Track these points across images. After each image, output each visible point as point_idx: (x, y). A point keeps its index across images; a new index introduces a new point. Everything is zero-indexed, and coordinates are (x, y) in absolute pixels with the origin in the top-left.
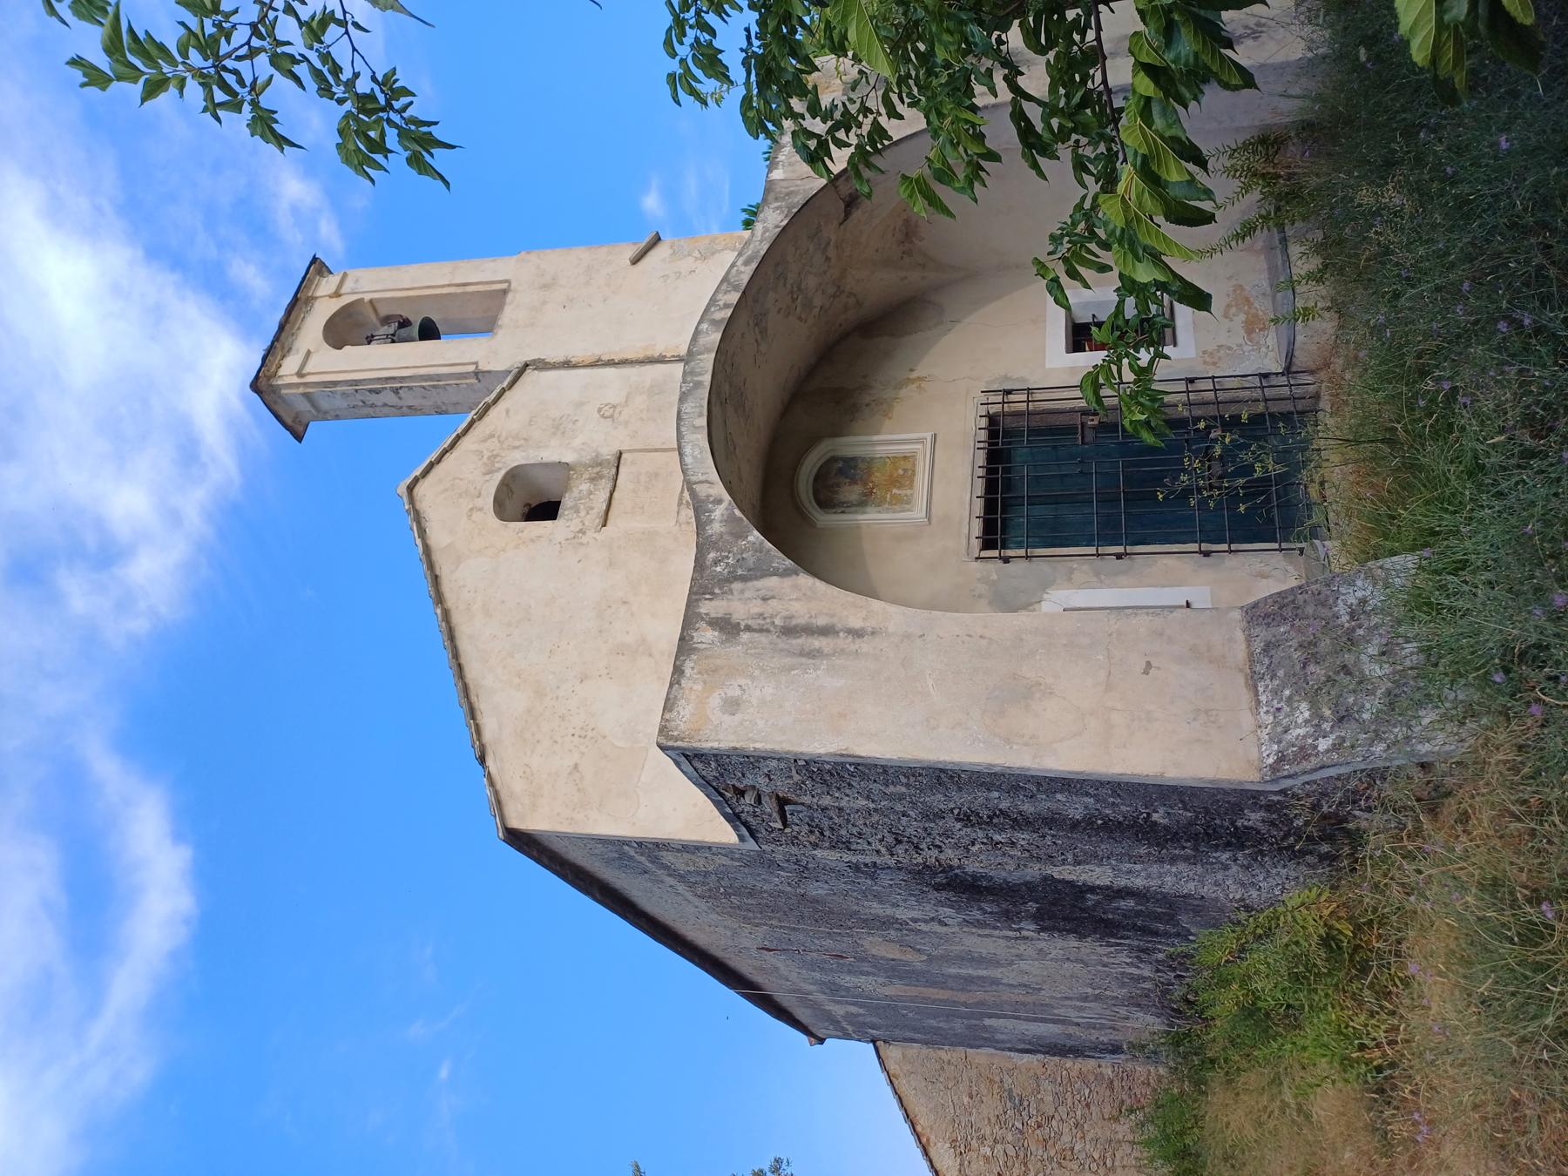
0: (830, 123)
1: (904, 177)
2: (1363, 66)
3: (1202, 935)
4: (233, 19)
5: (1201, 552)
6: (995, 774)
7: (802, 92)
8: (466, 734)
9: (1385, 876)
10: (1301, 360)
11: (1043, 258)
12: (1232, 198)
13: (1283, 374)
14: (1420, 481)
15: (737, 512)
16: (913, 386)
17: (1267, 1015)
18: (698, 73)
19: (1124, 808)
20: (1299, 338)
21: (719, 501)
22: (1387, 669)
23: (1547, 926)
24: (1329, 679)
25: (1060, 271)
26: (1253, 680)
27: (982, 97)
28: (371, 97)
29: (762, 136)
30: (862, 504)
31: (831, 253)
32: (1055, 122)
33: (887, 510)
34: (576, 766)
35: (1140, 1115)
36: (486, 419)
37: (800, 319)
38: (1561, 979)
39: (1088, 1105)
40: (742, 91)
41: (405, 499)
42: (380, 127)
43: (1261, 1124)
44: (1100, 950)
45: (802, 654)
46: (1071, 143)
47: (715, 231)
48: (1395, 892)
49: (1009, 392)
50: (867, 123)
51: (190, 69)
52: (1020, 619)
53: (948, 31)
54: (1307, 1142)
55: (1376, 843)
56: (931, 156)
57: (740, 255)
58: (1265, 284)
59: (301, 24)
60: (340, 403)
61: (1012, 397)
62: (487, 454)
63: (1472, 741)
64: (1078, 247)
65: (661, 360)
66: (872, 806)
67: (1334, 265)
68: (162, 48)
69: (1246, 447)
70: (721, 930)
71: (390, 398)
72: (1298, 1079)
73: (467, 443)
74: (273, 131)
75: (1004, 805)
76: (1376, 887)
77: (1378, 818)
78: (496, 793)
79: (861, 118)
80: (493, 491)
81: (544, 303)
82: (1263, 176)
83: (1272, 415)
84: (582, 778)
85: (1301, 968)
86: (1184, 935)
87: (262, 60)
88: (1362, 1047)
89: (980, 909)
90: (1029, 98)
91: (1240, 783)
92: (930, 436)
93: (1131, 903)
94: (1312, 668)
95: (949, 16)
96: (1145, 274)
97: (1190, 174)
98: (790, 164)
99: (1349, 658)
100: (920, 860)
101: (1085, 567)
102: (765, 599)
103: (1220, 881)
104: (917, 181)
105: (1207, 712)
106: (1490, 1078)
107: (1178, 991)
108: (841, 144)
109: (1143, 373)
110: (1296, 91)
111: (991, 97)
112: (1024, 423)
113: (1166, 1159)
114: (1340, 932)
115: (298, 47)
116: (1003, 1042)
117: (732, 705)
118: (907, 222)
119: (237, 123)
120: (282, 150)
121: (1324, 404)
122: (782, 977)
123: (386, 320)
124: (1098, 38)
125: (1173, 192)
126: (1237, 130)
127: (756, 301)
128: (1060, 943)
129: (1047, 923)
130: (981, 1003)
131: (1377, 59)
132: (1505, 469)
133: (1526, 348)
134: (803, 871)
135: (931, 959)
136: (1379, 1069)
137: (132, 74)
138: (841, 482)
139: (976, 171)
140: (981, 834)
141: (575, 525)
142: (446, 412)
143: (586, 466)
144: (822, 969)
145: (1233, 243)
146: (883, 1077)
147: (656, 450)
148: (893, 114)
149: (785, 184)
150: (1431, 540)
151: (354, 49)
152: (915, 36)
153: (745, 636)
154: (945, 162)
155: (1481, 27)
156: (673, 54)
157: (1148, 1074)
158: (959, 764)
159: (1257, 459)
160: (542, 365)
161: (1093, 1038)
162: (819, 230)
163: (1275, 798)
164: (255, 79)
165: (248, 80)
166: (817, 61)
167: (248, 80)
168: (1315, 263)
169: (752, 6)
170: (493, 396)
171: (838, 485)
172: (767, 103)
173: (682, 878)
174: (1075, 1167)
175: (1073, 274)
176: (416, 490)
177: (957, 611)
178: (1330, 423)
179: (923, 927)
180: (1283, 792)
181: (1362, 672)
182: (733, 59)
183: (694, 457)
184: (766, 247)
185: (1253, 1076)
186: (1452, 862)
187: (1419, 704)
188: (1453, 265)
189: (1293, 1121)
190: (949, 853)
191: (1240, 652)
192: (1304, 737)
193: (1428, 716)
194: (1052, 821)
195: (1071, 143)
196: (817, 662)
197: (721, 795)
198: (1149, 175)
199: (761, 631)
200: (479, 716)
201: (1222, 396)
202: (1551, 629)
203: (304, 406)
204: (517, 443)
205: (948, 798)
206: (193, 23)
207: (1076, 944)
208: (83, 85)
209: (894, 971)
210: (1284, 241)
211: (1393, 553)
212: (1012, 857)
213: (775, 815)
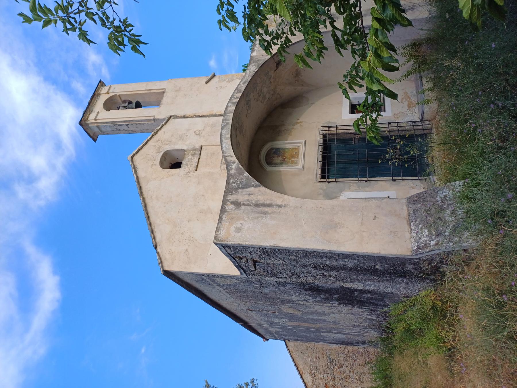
0: (272, 37)
1: (296, 55)
3: (392, 305)
5: (393, 180)
7: (263, 26)
8: (150, 239)
9: (452, 286)
10: (426, 117)
11: (342, 82)
12: (405, 63)
13: (420, 121)
15: (240, 166)
16: (298, 125)
17: (413, 331)
18: (228, 20)
19: (367, 264)
20: (426, 110)
21: (234, 162)
22: (453, 218)
23: (505, 303)
24: (434, 222)
26: (409, 222)
28: (119, 27)
29: (249, 41)
31: (272, 80)
32: (346, 37)
34: (187, 250)
36: (157, 135)
37: (261, 102)
38: (509, 320)
39: (355, 361)
41: (130, 161)
42: (122, 37)
43: (411, 367)
44: (359, 310)
45: (261, 213)
46: (351, 44)
47: (234, 73)
48: (455, 291)
49: (330, 127)
50: (284, 37)
51: (59, 17)
54: (426, 373)
56: (305, 48)
57: (242, 81)
58: (415, 92)
60: (109, 129)
61: (331, 129)
62: (157, 146)
64: (353, 79)
65: (215, 115)
66: (284, 263)
68: (49, 10)
70: (234, 304)
71: (126, 128)
72: (423, 353)
73: (150, 143)
75: (328, 263)
77: (450, 267)
78: (160, 259)
79: (282, 35)
80: (159, 158)
81: (177, 96)
82: (414, 56)
83: (416, 135)
86: (386, 306)
87: (83, 14)
88: (444, 342)
89: (320, 297)
91: (405, 256)
92: (304, 142)
93: (368, 295)
94: (429, 218)
96: (375, 87)
98: (259, 51)
99: (441, 215)
100: (300, 281)
101: (355, 185)
102: (249, 195)
103: (398, 288)
104: (300, 57)
105: (394, 232)
107: (384, 324)
108: (275, 44)
109: (374, 121)
110: (427, 28)
111: (325, 29)
113: (380, 379)
114: (437, 304)
115: (95, 10)
118: (297, 70)
119: (74, 35)
120: (89, 44)
121: (434, 131)
122: (255, 319)
123: (124, 102)
124: (360, 10)
125: (384, 60)
126: (407, 40)
127: (247, 96)
130: (320, 328)
131: (452, 17)
132: (492, 153)
133: (500, 113)
134: (262, 284)
135: (303, 313)
136: (450, 349)
137: (39, 19)
138: (275, 156)
139: (320, 53)
140: (320, 272)
141: (187, 170)
143: (190, 151)
145: (404, 78)
146: (287, 352)
147: (214, 145)
148: (293, 34)
149: (257, 57)
150: (468, 176)
151: (114, 11)
152: (300, 8)
153: (243, 207)
155: (486, 6)
156: (220, 14)
158: (313, 249)
159: (411, 149)
160: (176, 117)
163: (417, 261)
164: (80, 21)
165: (78, 21)
166: (268, 17)
167: (78, 21)
168: (431, 85)
170: (159, 127)
171: (274, 157)
172: (251, 30)
173: (222, 287)
174: (350, 381)
175: (351, 88)
176: (134, 158)
179: (301, 303)
180: (419, 259)
181: (445, 219)
182: (239, 15)
183: (226, 148)
184: (250, 78)
185: (409, 352)
186: (474, 281)
187: (464, 230)
188: (476, 86)
189: (422, 366)
190: (310, 278)
191: (405, 213)
192: (426, 241)
193: (467, 234)
194: (343, 268)
195: (351, 44)
196: (266, 216)
197: (235, 259)
198: (377, 54)
199: (248, 205)
200: (154, 233)
201: (400, 128)
202: (507, 205)
203: (97, 130)
204: (167, 143)
208: (23, 22)
209: (291, 317)
210: (421, 77)
212: (330, 280)
213: (253, 266)
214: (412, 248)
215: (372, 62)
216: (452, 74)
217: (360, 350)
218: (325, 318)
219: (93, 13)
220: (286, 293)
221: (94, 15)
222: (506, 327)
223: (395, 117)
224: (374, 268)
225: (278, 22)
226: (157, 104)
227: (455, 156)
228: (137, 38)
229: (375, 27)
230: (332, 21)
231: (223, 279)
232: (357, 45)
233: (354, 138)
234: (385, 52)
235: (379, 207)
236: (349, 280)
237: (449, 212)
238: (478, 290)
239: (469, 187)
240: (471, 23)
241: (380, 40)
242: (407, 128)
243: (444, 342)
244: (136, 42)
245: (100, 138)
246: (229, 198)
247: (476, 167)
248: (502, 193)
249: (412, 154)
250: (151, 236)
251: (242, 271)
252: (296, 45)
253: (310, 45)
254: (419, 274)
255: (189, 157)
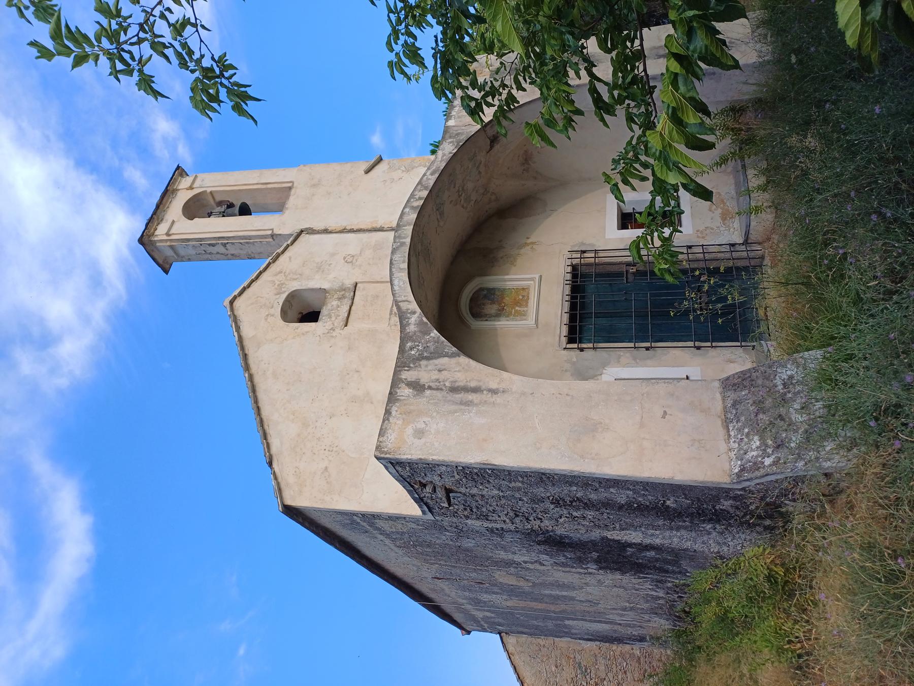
0: (483, 93)
1: (527, 123)
2: (791, 67)
4: (129, 21)
5: (695, 347)
6: (575, 476)
7: (467, 73)
8: (260, 448)
9: (803, 540)
10: (753, 237)
11: (609, 172)
13: (743, 244)
14: (825, 307)
15: (425, 319)
16: (528, 248)
17: (732, 620)
20: (753, 224)
21: (414, 313)
23: (900, 572)
25: (618, 179)
26: (726, 423)
27: (573, 81)
28: (211, 69)
29: (443, 99)
30: (498, 315)
31: (482, 169)
32: (616, 93)
33: (513, 320)
34: (326, 468)
35: (656, 679)
36: (277, 262)
37: (463, 207)
38: (909, 604)
39: (625, 672)
40: (431, 73)
41: (228, 309)
42: (215, 87)
44: (634, 581)
45: (461, 403)
46: (625, 105)
47: (413, 156)
48: (810, 549)
49: (584, 252)
50: (505, 93)
51: (102, 49)
52: (589, 385)
53: (553, 38)
55: (797, 521)
56: (543, 111)
57: (428, 169)
58: (733, 192)
59: (170, 25)
60: (192, 252)
61: (586, 255)
62: (277, 283)
63: (855, 461)
64: (628, 168)
65: (381, 230)
66: (501, 494)
67: (774, 181)
68: (85, 37)
69: (723, 286)
71: (222, 250)
72: (750, 659)
73: (265, 276)
74: (151, 88)
75: (579, 495)
76: (797, 546)
77: (800, 505)
79: (501, 90)
81: (313, 195)
82: (732, 129)
83: (737, 268)
84: (329, 476)
85: (754, 594)
86: (683, 573)
87: (146, 46)
89: (564, 556)
90: (599, 80)
91: (719, 483)
92: (538, 277)
93: (652, 554)
94: (761, 416)
95: (555, 30)
97: (701, 119)
98: (459, 117)
99: (782, 411)
101: (628, 355)
102: (440, 371)
103: (706, 541)
104: (535, 126)
105: (699, 441)
106: (866, 662)
107: (680, 606)
108: (489, 105)
109: (666, 241)
110: (754, 82)
111: (578, 80)
112: (593, 270)
115: (168, 38)
116: (576, 634)
117: (419, 434)
119: (130, 83)
120: (157, 99)
121: (767, 261)
123: (220, 204)
124: (641, 45)
128: (610, 576)
129: (604, 565)
131: (800, 62)
132: (875, 301)
133: (888, 230)
134: (460, 532)
135: (534, 585)
136: (800, 656)
137: (67, 52)
138: (486, 303)
140: (565, 512)
141: (329, 325)
142: (254, 258)
143: (336, 291)
144: (470, 591)
145: (715, 168)
146: (505, 655)
147: (378, 282)
150: (832, 342)
151: (201, 41)
152: (533, 43)
153: (428, 392)
154: (551, 114)
155: (889, 23)
156: (392, 50)
157: (662, 654)
159: (730, 293)
160: (311, 231)
161: (629, 632)
162: (475, 155)
164: (141, 57)
165: (137, 57)
166: (477, 57)
167: (137, 57)
168: (762, 180)
169: (438, 23)
170: (282, 249)
172: (447, 79)
173: (388, 536)
175: (626, 182)
176: (235, 304)
177: (553, 379)
178: (770, 273)
180: (743, 489)
181: (790, 419)
182: (427, 54)
187: (823, 438)
188: (844, 182)
190: (546, 523)
191: (718, 406)
192: (757, 457)
193: (829, 446)
194: (607, 504)
195: (625, 105)
196: (470, 408)
197: (412, 486)
198: (676, 119)
199: (437, 389)
201: (707, 256)
202: (904, 395)
203: (170, 253)
205: (547, 490)
206: (105, 22)
207: (620, 577)
208: (37, 58)
209: (512, 591)
211: (808, 350)
213: (444, 499)
214: (731, 470)
215: (667, 133)
216: (803, 161)
217: (634, 651)
218: (573, 594)
219: (164, 44)
220: (504, 548)
221: (165, 47)
222: (903, 616)
223: (698, 237)
224: (663, 505)
225: (494, 68)
226: (279, 208)
227: (807, 306)
228: (243, 89)
229: (672, 69)
230: (590, 65)
231: (390, 522)
232: (635, 107)
233: (627, 271)
234: (691, 114)
235: (672, 395)
236: (618, 526)
237: (797, 406)
238: (851, 548)
239: (834, 361)
240: (860, 54)
241: (681, 94)
242: (719, 255)
243: (790, 642)
244: (241, 97)
245: (176, 267)
246: (403, 377)
247: (845, 326)
248: (896, 372)
249: (730, 302)
250: (263, 443)
251: (425, 508)
252: (524, 108)
253: (553, 106)
254: (745, 515)
255: (333, 303)
